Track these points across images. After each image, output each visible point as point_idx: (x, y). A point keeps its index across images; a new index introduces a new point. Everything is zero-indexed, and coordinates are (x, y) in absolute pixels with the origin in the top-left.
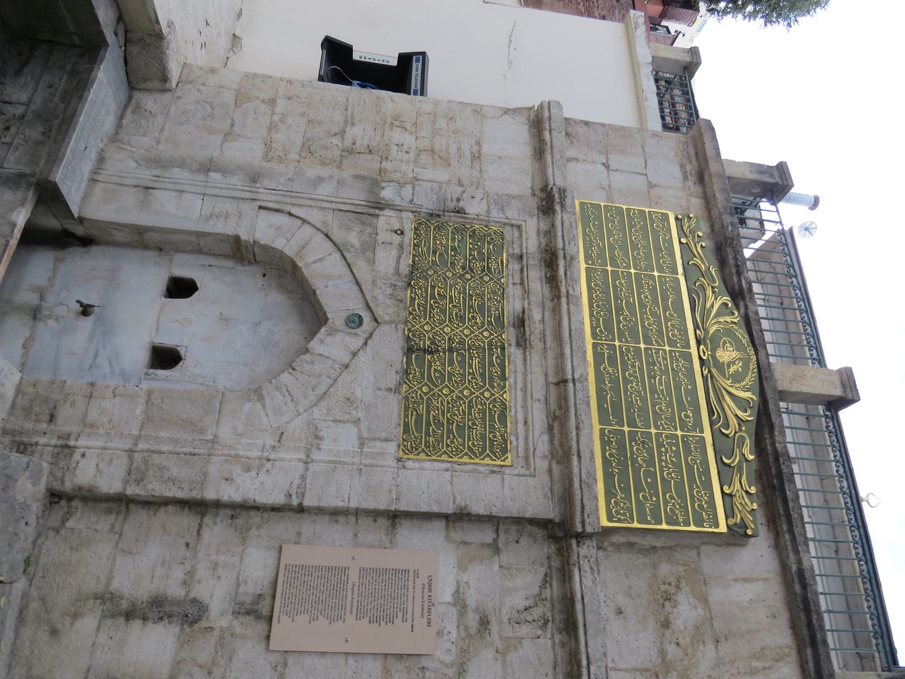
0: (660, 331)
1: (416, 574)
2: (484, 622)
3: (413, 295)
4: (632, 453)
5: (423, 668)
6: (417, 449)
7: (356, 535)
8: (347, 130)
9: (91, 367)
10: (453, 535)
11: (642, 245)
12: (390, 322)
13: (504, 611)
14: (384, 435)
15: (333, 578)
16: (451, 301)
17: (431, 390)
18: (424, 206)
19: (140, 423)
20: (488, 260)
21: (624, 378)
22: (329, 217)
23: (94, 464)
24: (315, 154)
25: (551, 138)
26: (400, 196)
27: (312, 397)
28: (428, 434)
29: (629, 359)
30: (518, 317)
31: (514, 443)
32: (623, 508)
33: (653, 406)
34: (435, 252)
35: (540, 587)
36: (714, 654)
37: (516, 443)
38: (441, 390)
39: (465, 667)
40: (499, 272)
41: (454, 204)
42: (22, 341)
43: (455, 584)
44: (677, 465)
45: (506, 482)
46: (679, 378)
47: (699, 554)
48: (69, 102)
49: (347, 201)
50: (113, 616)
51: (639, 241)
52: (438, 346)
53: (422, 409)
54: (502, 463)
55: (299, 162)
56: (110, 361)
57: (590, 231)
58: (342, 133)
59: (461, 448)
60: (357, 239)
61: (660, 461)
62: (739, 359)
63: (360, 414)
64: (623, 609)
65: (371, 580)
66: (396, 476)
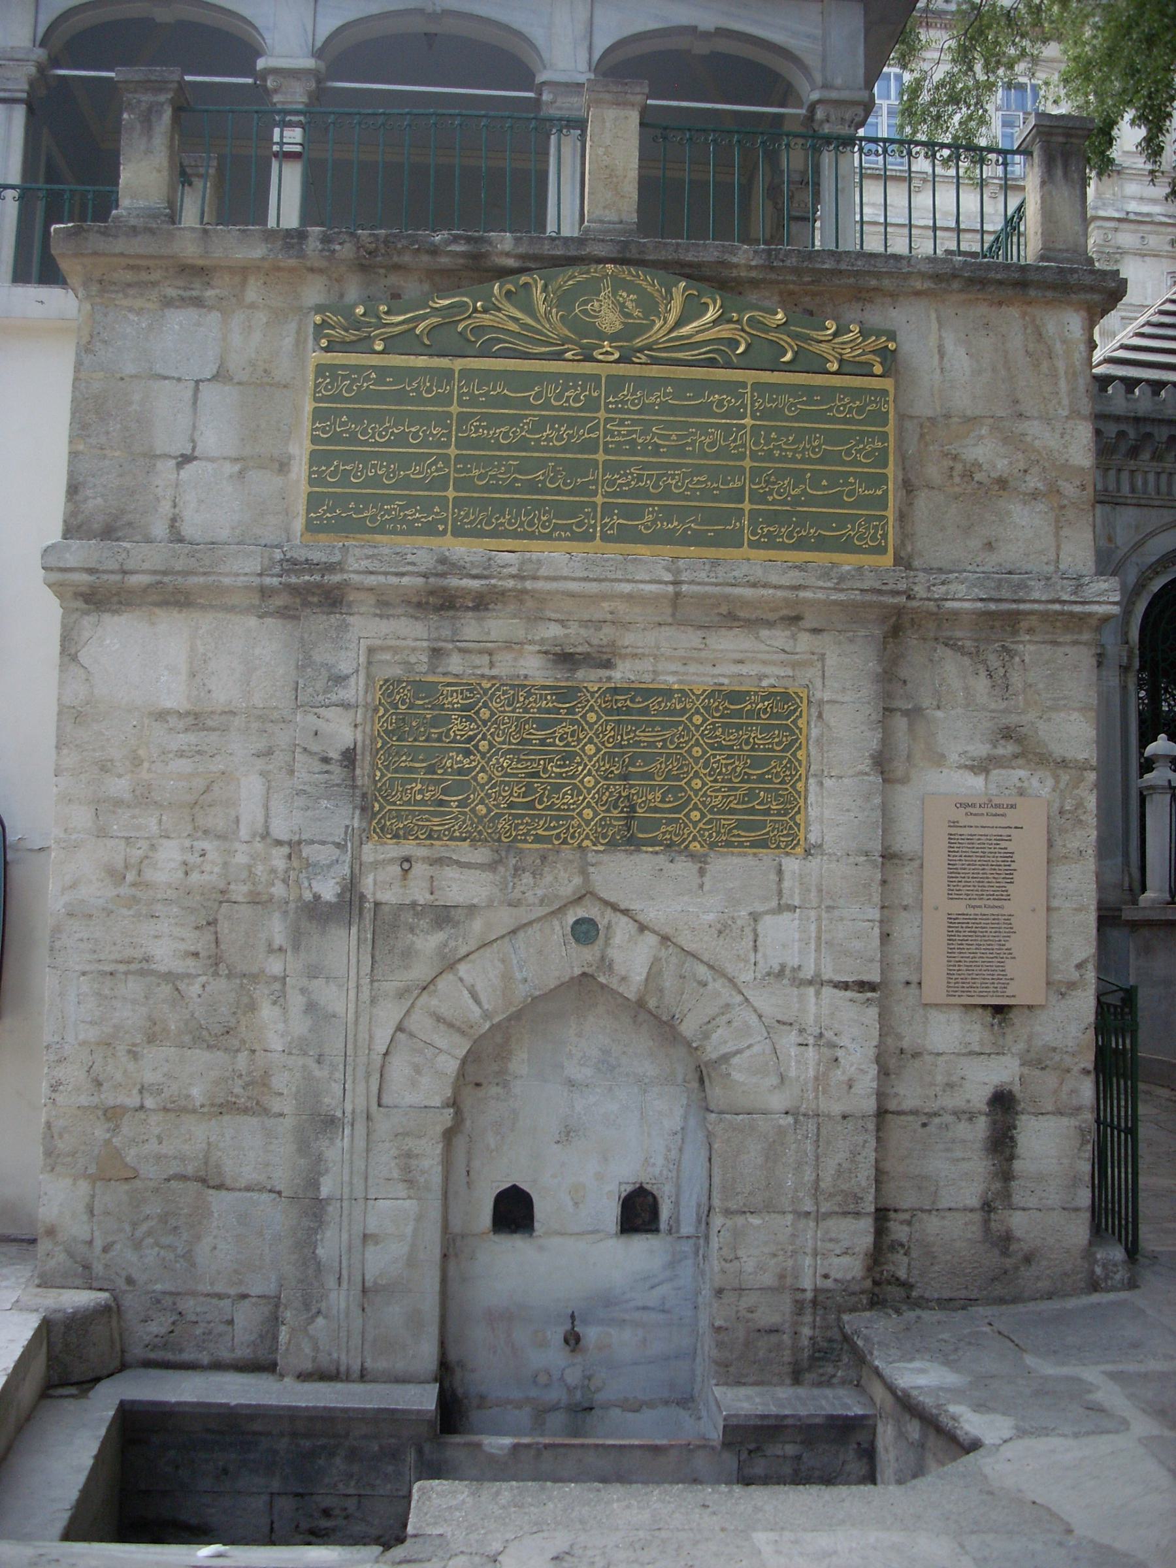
0: (572, 422)
1: (954, 824)
2: (1007, 734)
3: (530, 839)
4: (784, 503)
6: (791, 828)
7: (905, 908)
8: (163, 968)
9: (663, 1311)
10: (899, 773)
11: (396, 426)
12: (583, 872)
13: (993, 706)
14: (773, 877)
16: (535, 775)
17: (695, 808)
18: (347, 822)
19: (773, 1216)
20: (448, 710)
21: (660, 496)
22: (390, 986)
23: (836, 1260)
24: (232, 1025)
25: (144, 572)
26: (330, 866)
27: (718, 985)
28: (767, 812)
29: (628, 484)
30: (555, 662)
31: (772, 681)
32: (867, 529)
33: (705, 456)
34: (441, 803)
35: (962, 655)
36: (1036, 423)
37: (773, 676)
38: (696, 792)
40: (471, 691)
41: (336, 769)
42: (630, 1415)
43: (961, 771)
44: (801, 434)
45: (834, 697)
46: (654, 404)
47: (911, 417)
48: (255, 1433)
49: (353, 960)
50: (1009, 1196)
51: (386, 429)
52: (620, 797)
53: (728, 820)
54: (805, 701)
55: (254, 1051)
56: (652, 1288)
57: (373, 518)
58: (170, 977)
59: (784, 762)
60: (429, 937)
61: (794, 460)
62: (614, 293)
63: (743, 913)
64: (986, 541)
66: (834, 858)
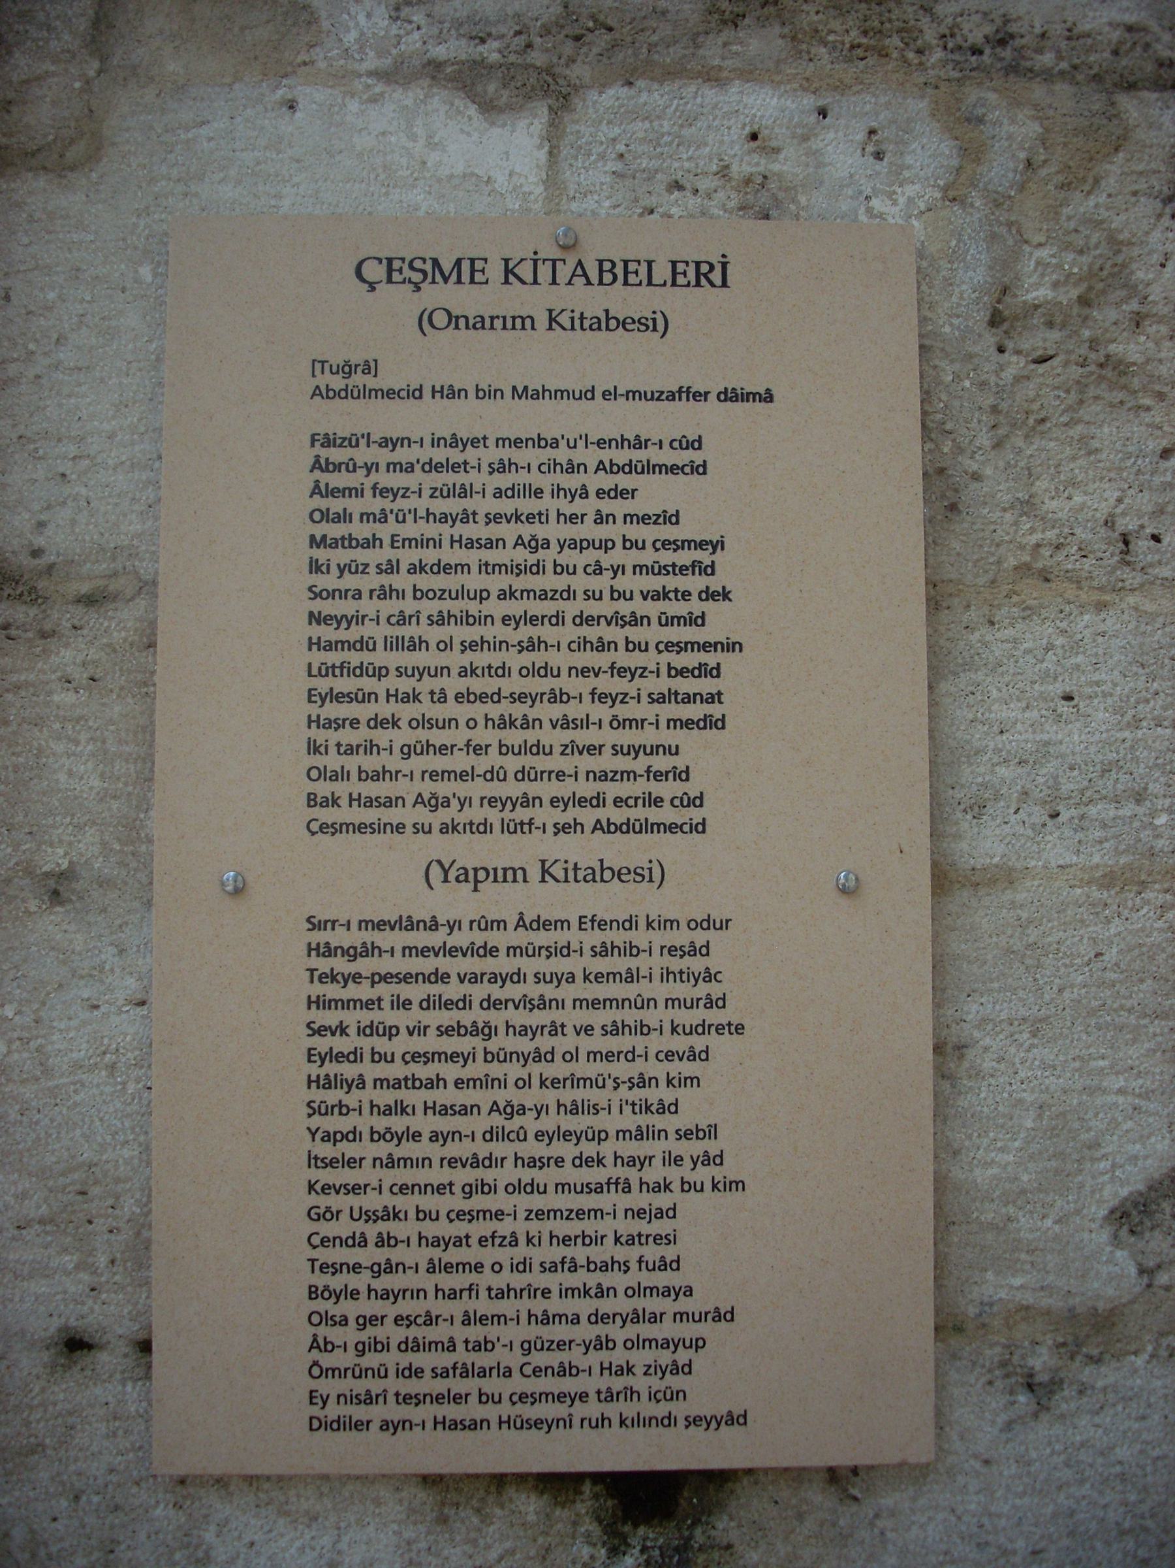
5: (995, 320)
15: (402, 1044)
39: (975, 32)
43: (408, 97)
65: (403, 736)
